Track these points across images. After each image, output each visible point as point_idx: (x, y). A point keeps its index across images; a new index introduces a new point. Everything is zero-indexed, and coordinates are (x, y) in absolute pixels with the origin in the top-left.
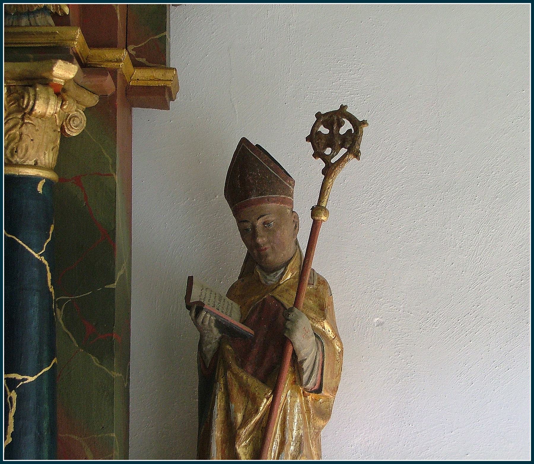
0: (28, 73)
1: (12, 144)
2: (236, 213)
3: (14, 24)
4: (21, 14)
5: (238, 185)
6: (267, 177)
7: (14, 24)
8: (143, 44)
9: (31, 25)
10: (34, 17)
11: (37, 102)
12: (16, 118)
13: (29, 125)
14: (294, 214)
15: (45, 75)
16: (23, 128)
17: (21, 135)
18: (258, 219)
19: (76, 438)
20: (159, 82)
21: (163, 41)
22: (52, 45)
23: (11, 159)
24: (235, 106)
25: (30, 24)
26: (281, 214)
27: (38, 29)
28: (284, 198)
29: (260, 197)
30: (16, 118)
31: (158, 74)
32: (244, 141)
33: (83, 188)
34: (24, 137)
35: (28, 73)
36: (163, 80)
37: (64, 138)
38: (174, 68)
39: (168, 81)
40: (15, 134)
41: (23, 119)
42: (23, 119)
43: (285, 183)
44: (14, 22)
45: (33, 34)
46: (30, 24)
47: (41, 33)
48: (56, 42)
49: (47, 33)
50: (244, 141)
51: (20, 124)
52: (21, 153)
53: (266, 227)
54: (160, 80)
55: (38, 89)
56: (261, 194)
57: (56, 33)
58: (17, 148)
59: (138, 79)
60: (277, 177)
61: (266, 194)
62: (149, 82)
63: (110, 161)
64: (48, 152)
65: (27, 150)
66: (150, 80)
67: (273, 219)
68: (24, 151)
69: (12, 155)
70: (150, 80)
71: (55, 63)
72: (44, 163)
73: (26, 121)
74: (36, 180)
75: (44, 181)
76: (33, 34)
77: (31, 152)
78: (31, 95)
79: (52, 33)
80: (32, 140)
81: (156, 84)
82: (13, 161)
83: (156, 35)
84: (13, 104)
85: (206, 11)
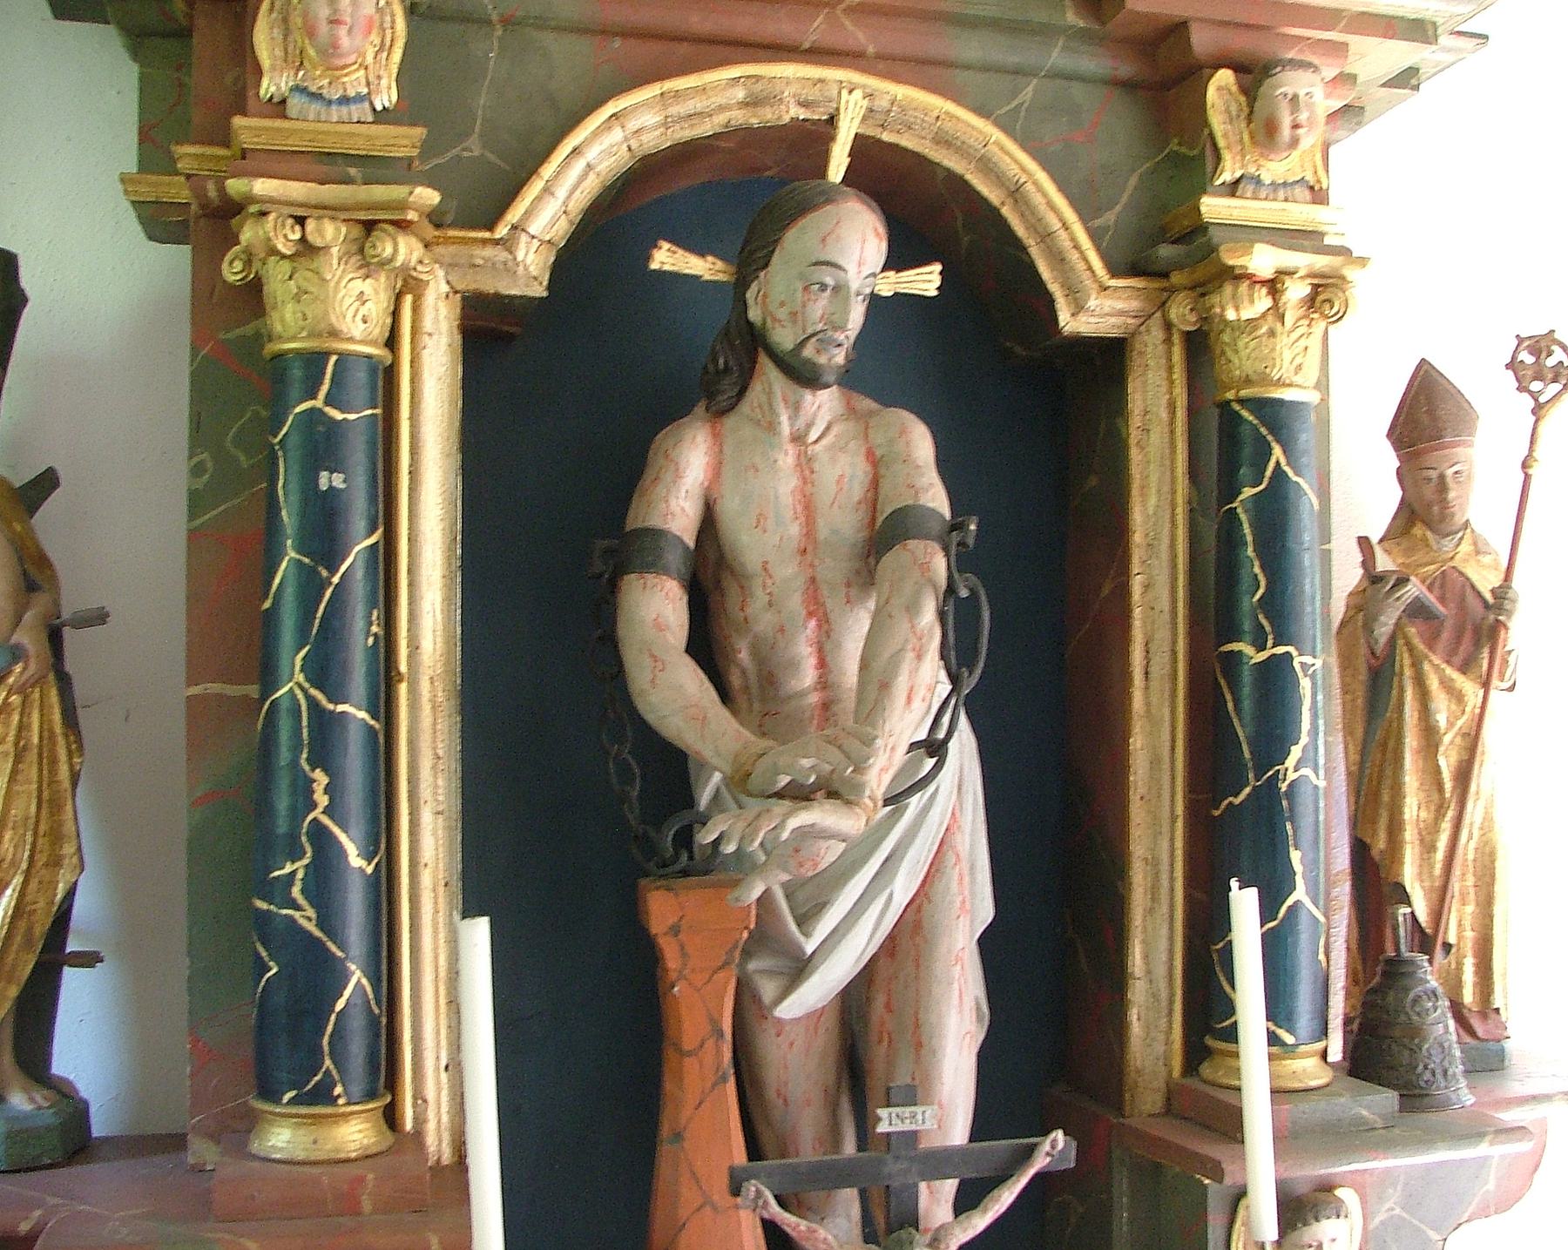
19: (502, 165)
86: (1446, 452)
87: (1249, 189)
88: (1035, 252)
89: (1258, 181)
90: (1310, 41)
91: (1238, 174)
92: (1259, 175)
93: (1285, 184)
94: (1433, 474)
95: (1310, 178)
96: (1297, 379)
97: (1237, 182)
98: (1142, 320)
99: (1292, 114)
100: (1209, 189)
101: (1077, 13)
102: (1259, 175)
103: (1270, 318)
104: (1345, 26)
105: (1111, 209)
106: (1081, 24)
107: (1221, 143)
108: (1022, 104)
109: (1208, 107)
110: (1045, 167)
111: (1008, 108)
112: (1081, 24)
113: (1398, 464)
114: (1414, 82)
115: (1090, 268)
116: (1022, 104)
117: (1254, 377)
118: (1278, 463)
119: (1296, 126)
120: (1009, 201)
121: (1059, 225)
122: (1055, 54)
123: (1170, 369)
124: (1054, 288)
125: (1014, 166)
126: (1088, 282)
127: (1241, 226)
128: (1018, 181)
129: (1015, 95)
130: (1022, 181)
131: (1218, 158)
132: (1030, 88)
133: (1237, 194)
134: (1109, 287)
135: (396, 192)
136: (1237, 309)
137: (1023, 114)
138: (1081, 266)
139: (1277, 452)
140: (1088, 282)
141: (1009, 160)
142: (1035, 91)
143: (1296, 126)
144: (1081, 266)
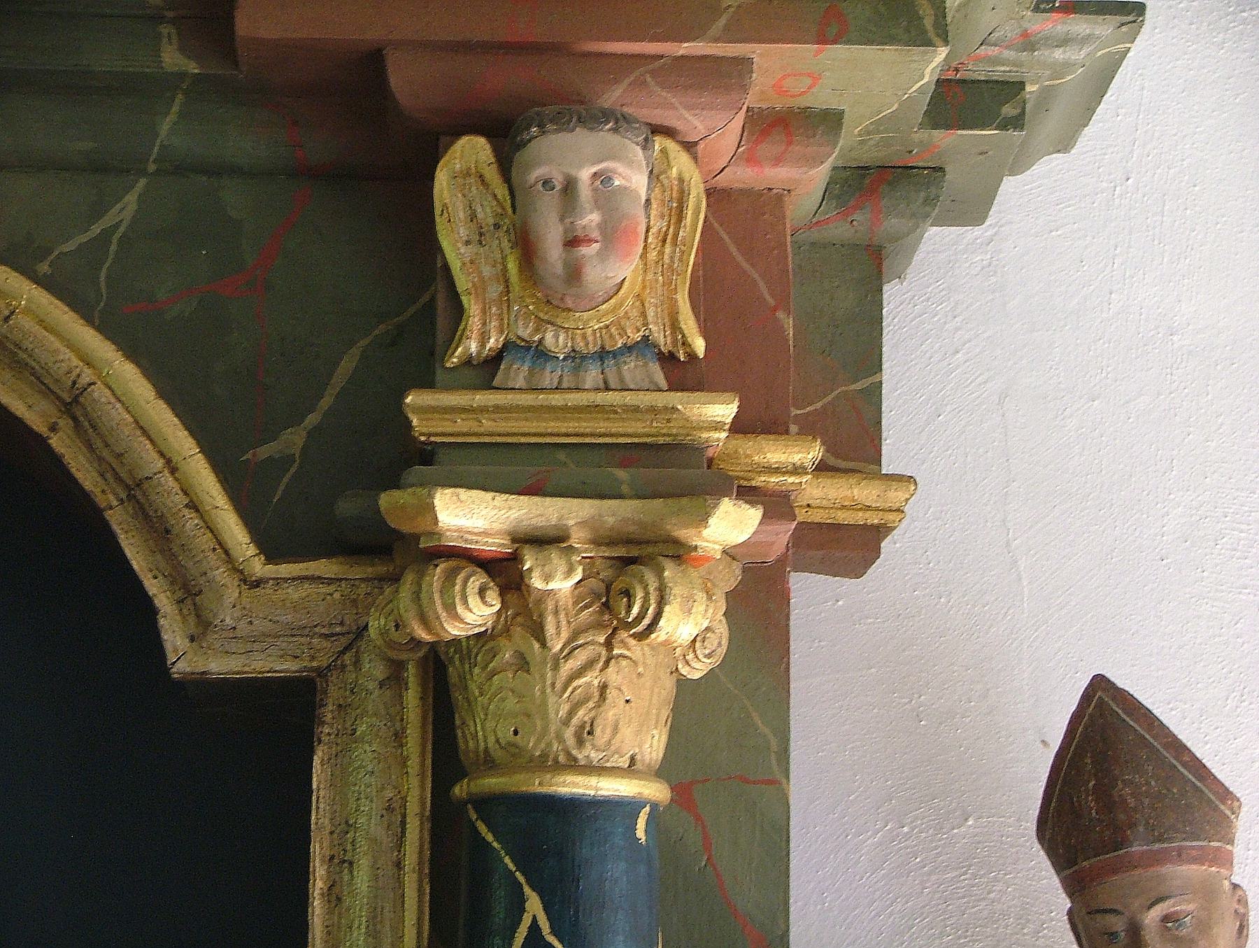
0: (636, 527)
1: (581, 713)
2: (1075, 885)
3: (565, 385)
4: (584, 358)
5: (1092, 809)
6: (1175, 791)
7: (565, 385)
8: (819, 405)
9: (607, 389)
10: (617, 364)
11: (667, 609)
12: (592, 643)
13: (624, 663)
14: (1240, 893)
15: (683, 534)
16: (610, 669)
17: (603, 688)
18: (1149, 908)
20: (868, 514)
21: (874, 395)
22: (661, 440)
23: (574, 752)
24: (1019, 563)
25: (605, 382)
26: (1208, 893)
27: (629, 398)
28: (1218, 849)
29: (1157, 846)
30: (592, 643)
31: (865, 492)
32: (1100, 684)
33: (698, 818)
34: (611, 694)
35: (636, 527)
36: (877, 509)
37: (683, 684)
38: (912, 477)
39: (890, 511)
40: (589, 684)
41: (609, 644)
42: (609, 644)
43: (1222, 807)
44: (565, 379)
45: (616, 412)
46: (605, 382)
47: (636, 409)
48: (674, 431)
49: (653, 410)
50: (1100, 684)
51: (603, 659)
52: (601, 735)
53: (1169, 929)
54: (868, 508)
55: (666, 574)
56: (1160, 839)
57: (674, 409)
58: (591, 725)
59: (808, 505)
60: (1202, 791)
61: (1170, 840)
62: (839, 513)
63: (774, 742)
64: (659, 731)
65: (616, 729)
66: (843, 507)
67: (1191, 907)
68: (608, 731)
69: (580, 743)
70: (843, 507)
71: (716, 506)
72: (647, 761)
73: (616, 652)
74: (628, 808)
75: (648, 808)
76: (616, 412)
77: (626, 732)
78: (651, 589)
79: (666, 408)
80: (627, 701)
81: (859, 518)
82: (580, 756)
83: (856, 381)
84: (586, 607)
85: (937, 291)
86: (1152, 871)
87: (517, 371)
88: (118, 519)
89: (541, 354)
90: (657, 64)
91: (493, 342)
92: (541, 341)
93: (603, 355)
94: (1118, 924)
95: (662, 338)
96: (590, 753)
97: (495, 360)
98: (344, 641)
99: (562, 219)
100: (440, 375)
101: (182, 49)
102: (541, 341)
103: (517, 631)
104: (727, 28)
105: (296, 420)
106: (193, 68)
107: (462, 283)
108: (117, 226)
109: (437, 212)
110: (132, 353)
111: (83, 238)
112: (193, 68)
113: (1068, 904)
114: (1008, 110)
115: (222, 546)
116: (117, 226)
117: (498, 754)
118: (534, 927)
119: (572, 242)
120: (65, 423)
121: (160, 463)
122: (165, 127)
123: (399, 737)
124: (156, 589)
125: (66, 354)
126: (221, 574)
127: (503, 444)
128: (74, 383)
129: (98, 211)
130: (85, 380)
131: (458, 311)
132: (131, 199)
133: (495, 383)
134: (266, 581)
135: (66, 317)
136: (457, 617)
137: (113, 247)
138: (204, 541)
139: (534, 905)
140: (221, 574)
141: (57, 344)
142: (142, 199)
143: (572, 242)
144: (204, 541)
